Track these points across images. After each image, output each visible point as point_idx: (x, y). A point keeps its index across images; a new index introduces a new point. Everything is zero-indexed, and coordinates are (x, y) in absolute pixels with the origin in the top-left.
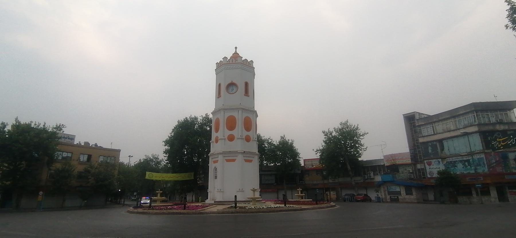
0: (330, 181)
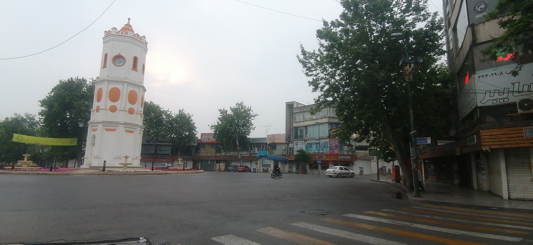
0: (223, 154)
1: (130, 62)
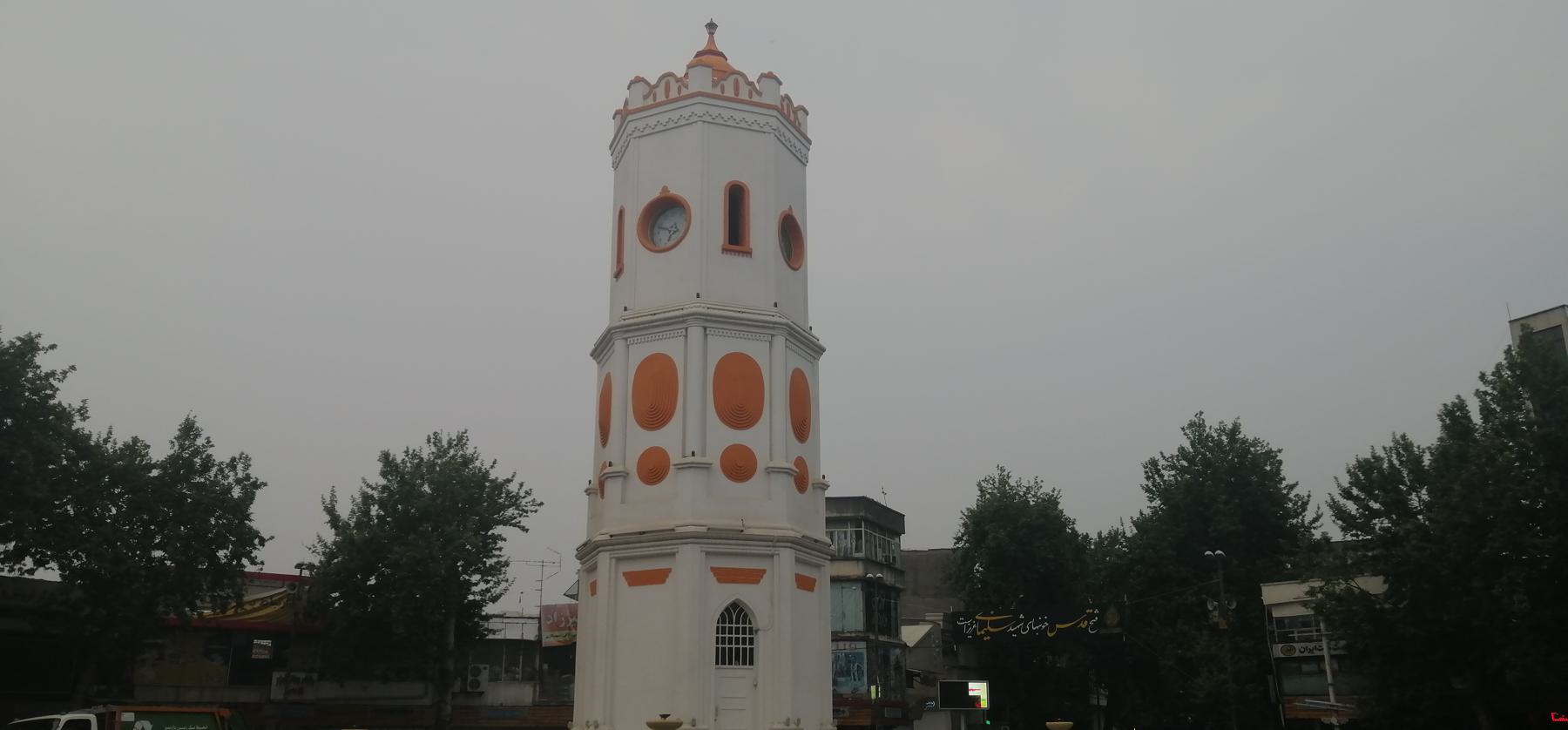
1: (709, 217)
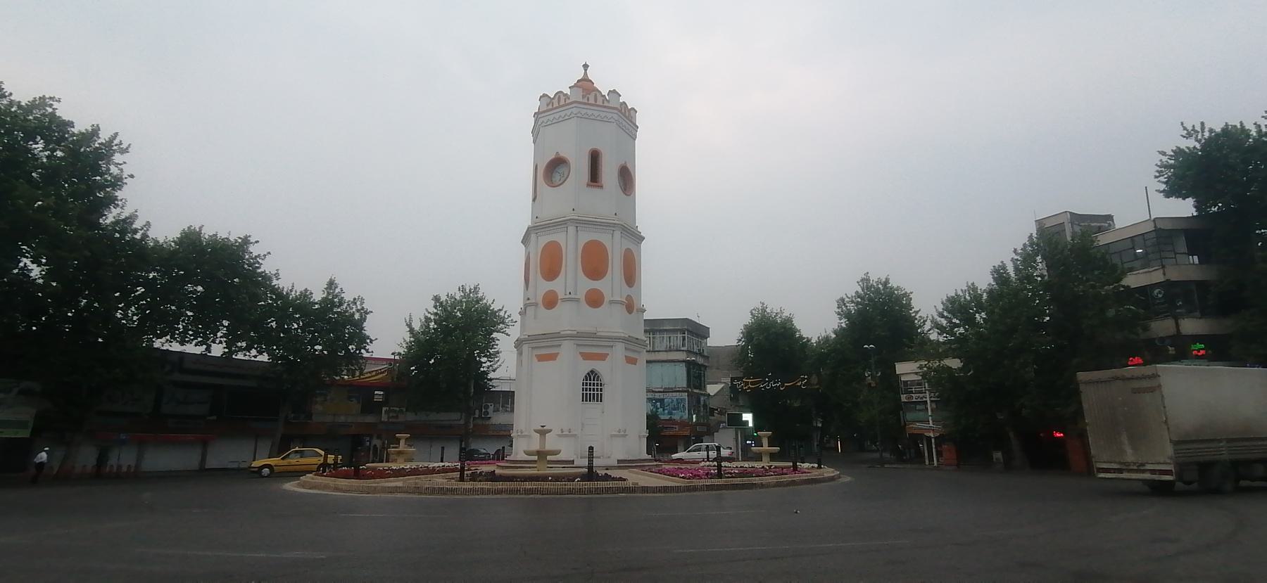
1: (580, 167)
